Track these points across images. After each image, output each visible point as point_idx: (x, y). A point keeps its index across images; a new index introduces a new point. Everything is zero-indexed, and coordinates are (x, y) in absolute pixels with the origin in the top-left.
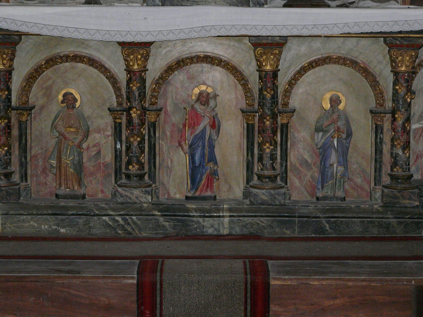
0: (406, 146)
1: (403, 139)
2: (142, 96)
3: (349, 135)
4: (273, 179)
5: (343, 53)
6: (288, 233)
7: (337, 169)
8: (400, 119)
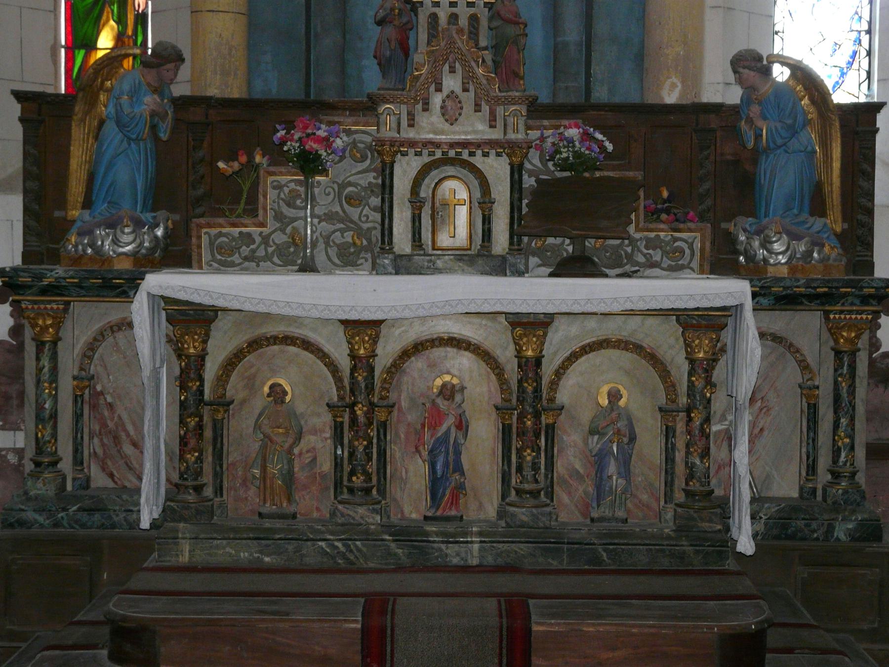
0: (705, 453)
1: (701, 444)
2: (370, 388)
3: (633, 439)
4: (535, 494)
5: (624, 334)
6: (555, 564)
8: (697, 418)
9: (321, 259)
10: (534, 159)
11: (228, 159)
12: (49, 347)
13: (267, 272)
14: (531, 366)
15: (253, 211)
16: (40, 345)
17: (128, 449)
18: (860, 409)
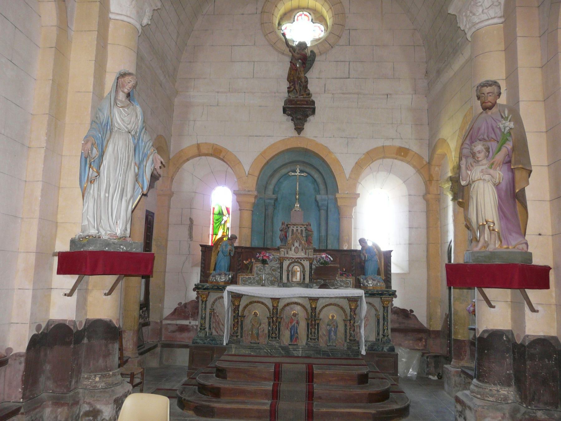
0: (354, 331)
1: (353, 328)
2: (277, 314)
3: (337, 327)
4: (314, 339)
5: (335, 302)
6: (319, 356)
7: (333, 337)
8: (352, 322)
9: (266, 283)
10: (315, 262)
11: (246, 261)
12: (205, 302)
13: (255, 286)
14: (314, 309)
15: (251, 272)
16: (203, 301)
17: (221, 326)
18: (389, 320)
